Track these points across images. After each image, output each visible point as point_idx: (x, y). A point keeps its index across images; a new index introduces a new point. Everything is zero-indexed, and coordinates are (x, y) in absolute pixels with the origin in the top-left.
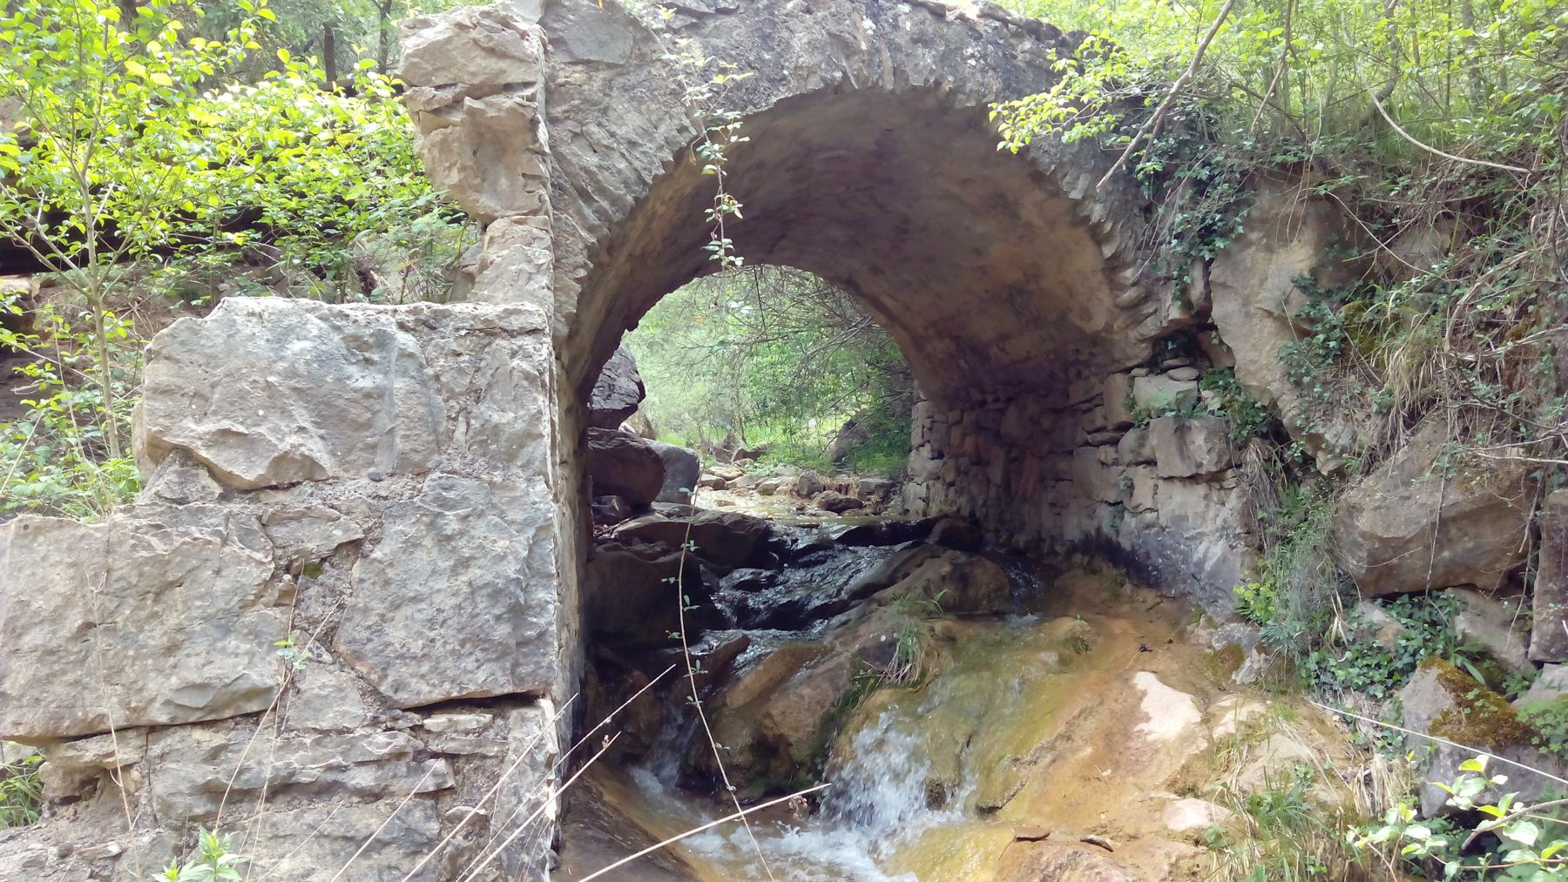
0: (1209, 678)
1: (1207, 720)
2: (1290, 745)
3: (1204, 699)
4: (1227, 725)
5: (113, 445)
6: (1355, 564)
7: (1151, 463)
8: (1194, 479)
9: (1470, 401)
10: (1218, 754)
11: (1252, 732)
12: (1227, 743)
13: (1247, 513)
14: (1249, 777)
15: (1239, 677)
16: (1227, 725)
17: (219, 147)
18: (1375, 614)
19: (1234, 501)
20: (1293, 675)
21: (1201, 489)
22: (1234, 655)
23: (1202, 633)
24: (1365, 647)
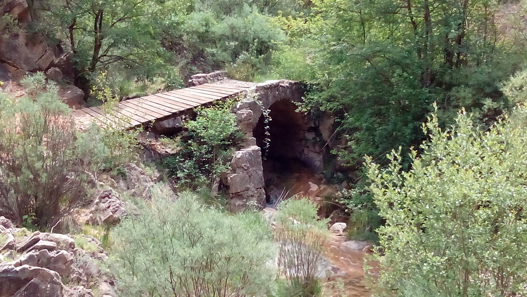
0: (318, 182)
1: (319, 188)
2: (329, 190)
3: (318, 185)
4: (322, 189)
5: (474, 128)
6: (337, 167)
7: (308, 147)
8: (315, 152)
9: (376, 144)
10: (321, 192)
11: (325, 189)
12: (322, 190)
13: (323, 158)
14: (325, 194)
15: (322, 182)
16: (322, 189)
17: (509, 12)
18: (340, 174)
19: (321, 156)
20: (329, 182)
21: (316, 154)
22: (321, 179)
23: (316, 176)
24: (338, 178)
